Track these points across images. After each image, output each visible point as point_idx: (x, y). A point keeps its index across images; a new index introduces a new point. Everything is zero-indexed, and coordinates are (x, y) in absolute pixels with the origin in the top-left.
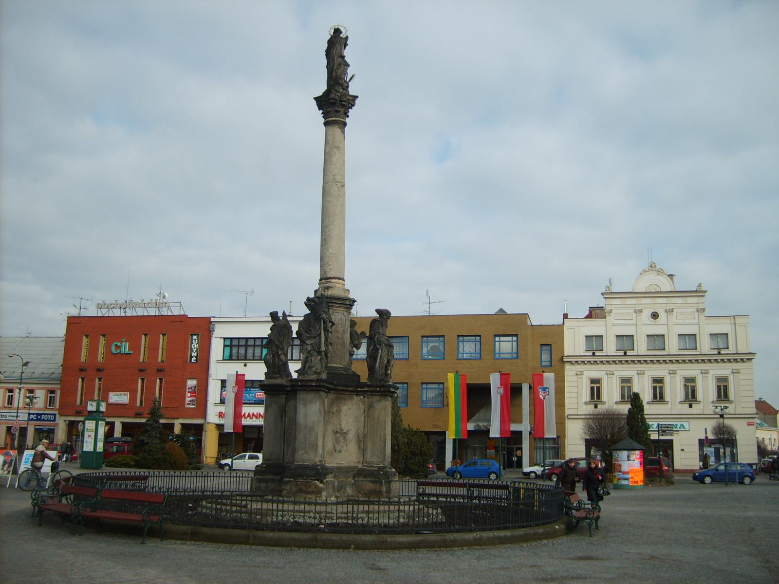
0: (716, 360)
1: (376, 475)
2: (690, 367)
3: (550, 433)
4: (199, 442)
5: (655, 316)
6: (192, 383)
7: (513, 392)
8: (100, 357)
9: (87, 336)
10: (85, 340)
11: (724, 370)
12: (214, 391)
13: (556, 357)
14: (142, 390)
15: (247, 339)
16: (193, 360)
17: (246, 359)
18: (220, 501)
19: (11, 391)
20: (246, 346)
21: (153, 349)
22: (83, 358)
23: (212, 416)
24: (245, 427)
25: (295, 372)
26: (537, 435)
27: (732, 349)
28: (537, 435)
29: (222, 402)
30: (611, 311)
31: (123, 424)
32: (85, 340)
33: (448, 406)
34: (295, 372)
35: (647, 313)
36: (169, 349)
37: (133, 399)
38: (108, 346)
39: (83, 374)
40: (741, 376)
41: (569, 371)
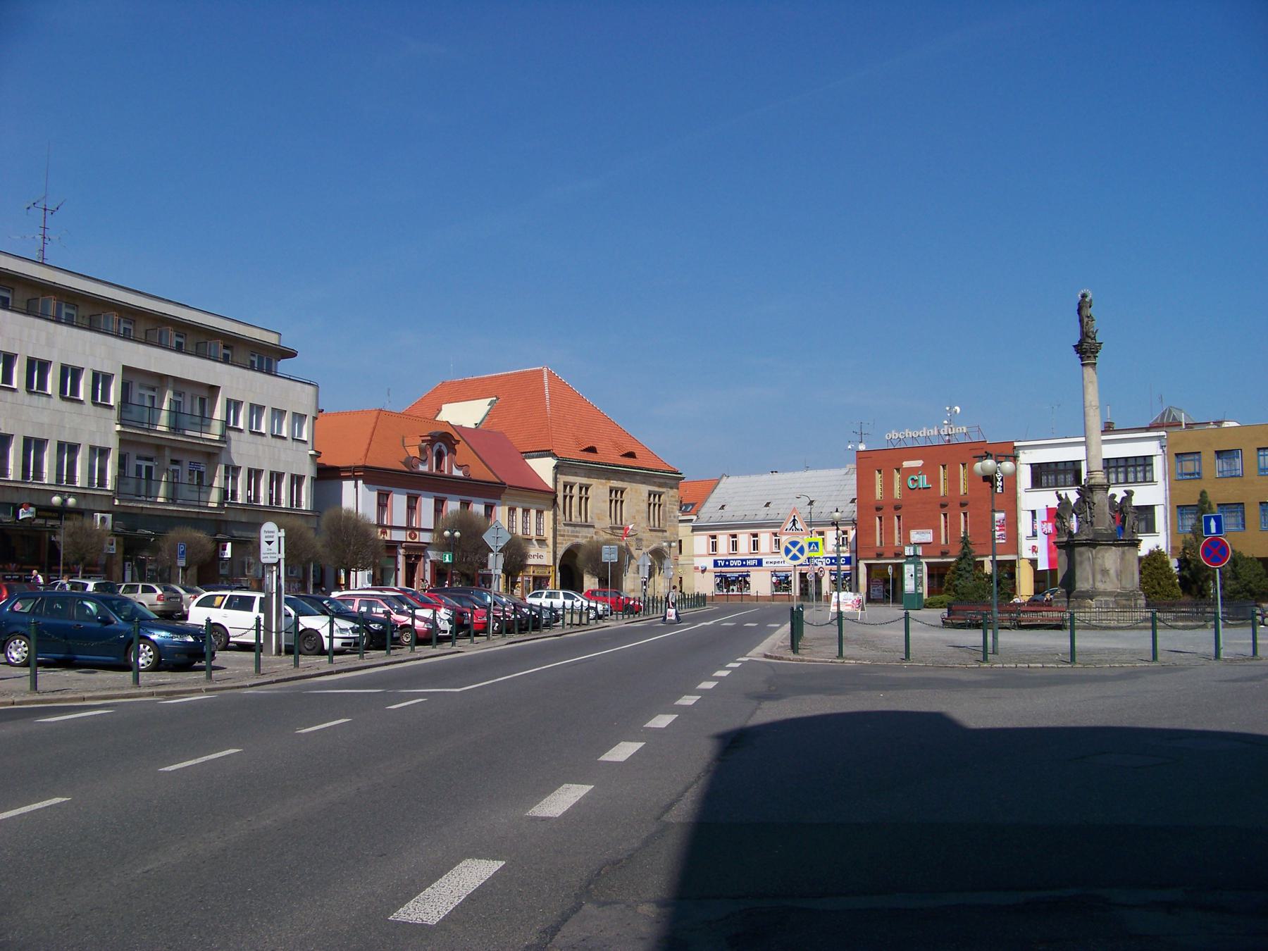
1: (1129, 596)
2: (184, 683)
4: (1012, 576)
6: (999, 516)
8: (897, 494)
9: (880, 471)
10: (878, 476)
12: (1024, 527)
15: (1126, 459)
16: (999, 490)
19: (755, 535)
20: (1126, 467)
22: (878, 496)
23: (1026, 553)
25: (1203, 493)
29: (1035, 535)
32: (878, 476)
34: (1203, 493)
37: (937, 536)
38: (903, 481)
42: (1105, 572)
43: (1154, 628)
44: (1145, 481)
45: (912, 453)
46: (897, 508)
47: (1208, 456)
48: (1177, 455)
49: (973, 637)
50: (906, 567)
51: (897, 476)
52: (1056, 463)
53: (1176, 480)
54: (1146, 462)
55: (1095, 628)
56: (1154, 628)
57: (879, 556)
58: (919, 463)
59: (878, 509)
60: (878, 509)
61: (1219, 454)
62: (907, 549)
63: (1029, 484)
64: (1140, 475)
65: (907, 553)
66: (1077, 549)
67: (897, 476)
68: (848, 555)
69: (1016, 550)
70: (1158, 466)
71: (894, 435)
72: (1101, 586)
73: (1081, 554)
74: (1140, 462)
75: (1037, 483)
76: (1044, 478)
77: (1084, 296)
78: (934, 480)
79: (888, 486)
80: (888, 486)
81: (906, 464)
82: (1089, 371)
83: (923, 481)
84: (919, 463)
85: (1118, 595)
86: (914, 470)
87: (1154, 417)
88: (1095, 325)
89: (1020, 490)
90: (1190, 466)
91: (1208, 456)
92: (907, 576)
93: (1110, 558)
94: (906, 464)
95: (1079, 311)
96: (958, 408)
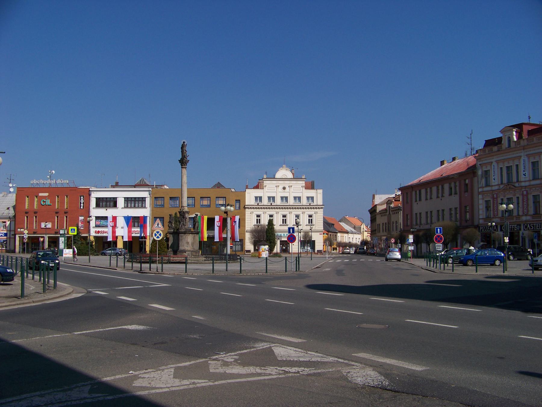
0: (308, 208)
1: (196, 252)
3: (237, 238)
5: (284, 188)
7: (224, 221)
9: (28, 197)
10: (27, 199)
11: (311, 212)
13: (242, 207)
14: (58, 221)
15: (135, 198)
16: (82, 207)
17: (106, 207)
18: (490, 224)
20: (135, 201)
21: (62, 203)
22: (27, 207)
24: (133, 237)
26: (233, 238)
27: (315, 203)
28: (233, 238)
30: (266, 186)
31: (49, 237)
32: (27, 199)
33: (529, 241)
35: (281, 187)
36: (69, 203)
38: (39, 202)
39: (57, 215)
40: (318, 215)
41: (248, 211)
42: (188, 243)
43: (213, 263)
44: (142, 207)
45: (43, 190)
46: (35, 213)
47: (167, 199)
48: (170, 198)
49: (137, 265)
50: (60, 238)
51: (36, 199)
52: (107, 198)
53: (154, 207)
54: (143, 200)
55: (200, 263)
56: (213, 263)
57: (35, 233)
58: (47, 194)
59: (26, 213)
60: (26, 213)
61: (171, 198)
62: (61, 231)
63: (95, 206)
64: (140, 205)
65: (61, 233)
66: (180, 235)
67: (36, 199)
68: (6, 232)
69: (89, 231)
70: (148, 201)
71: (35, 182)
72: (187, 248)
73: (182, 236)
74: (141, 199)
75: (98, 205)
76: (101, 204)
77: (184, 142)
78: (53, 202)
79: (31, 203)
80: (31, 203)
81: (41, 194)
82: (184, 170)
83: (48, 202)
84: (47, 194)
85: (192, 251)
86: (44, 197)
87: (137, 182)
88: (188, 153)
89: (91, 208)
90: (160, 202)
91: (167, 199)
92: (61, 242)
93: (189, 238)
94: (41, 194)
95: (182, 148)
96: (54, 172)
